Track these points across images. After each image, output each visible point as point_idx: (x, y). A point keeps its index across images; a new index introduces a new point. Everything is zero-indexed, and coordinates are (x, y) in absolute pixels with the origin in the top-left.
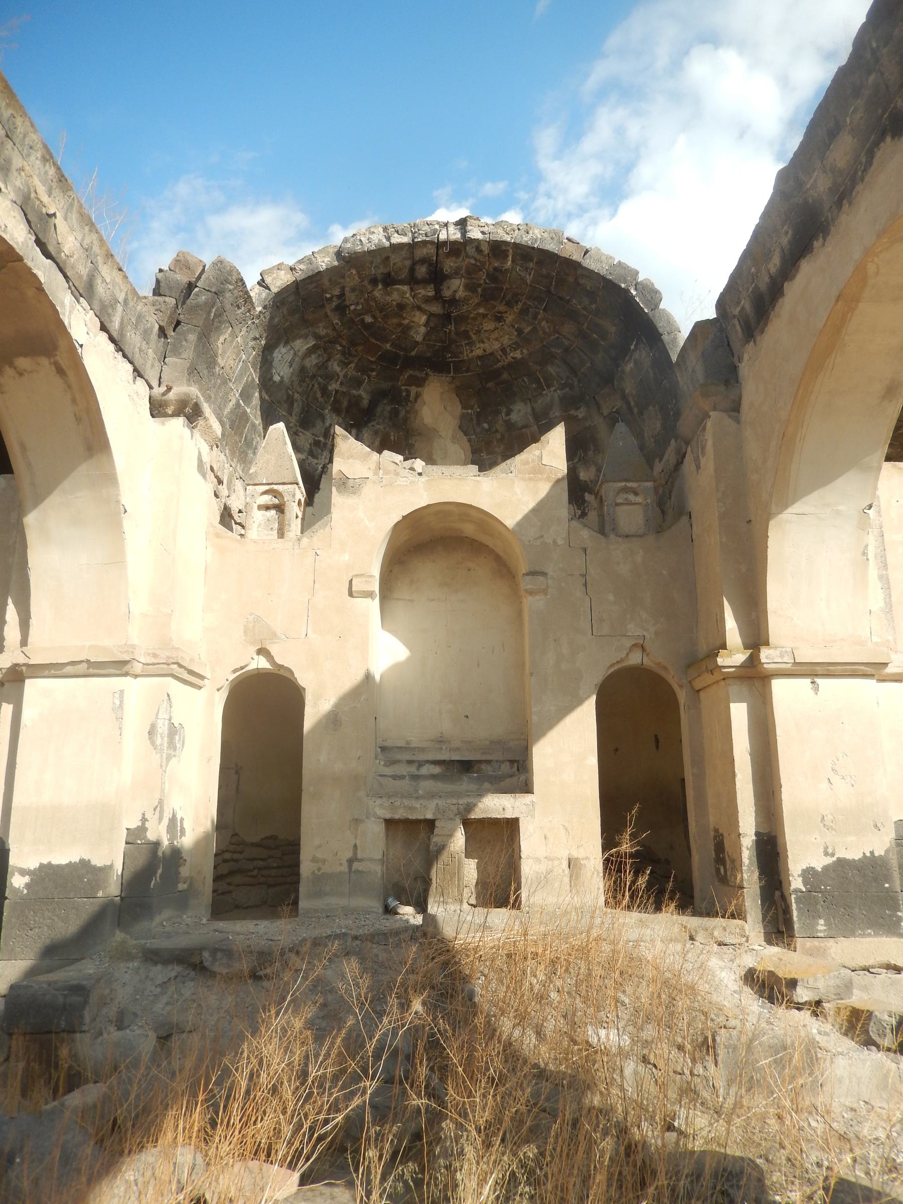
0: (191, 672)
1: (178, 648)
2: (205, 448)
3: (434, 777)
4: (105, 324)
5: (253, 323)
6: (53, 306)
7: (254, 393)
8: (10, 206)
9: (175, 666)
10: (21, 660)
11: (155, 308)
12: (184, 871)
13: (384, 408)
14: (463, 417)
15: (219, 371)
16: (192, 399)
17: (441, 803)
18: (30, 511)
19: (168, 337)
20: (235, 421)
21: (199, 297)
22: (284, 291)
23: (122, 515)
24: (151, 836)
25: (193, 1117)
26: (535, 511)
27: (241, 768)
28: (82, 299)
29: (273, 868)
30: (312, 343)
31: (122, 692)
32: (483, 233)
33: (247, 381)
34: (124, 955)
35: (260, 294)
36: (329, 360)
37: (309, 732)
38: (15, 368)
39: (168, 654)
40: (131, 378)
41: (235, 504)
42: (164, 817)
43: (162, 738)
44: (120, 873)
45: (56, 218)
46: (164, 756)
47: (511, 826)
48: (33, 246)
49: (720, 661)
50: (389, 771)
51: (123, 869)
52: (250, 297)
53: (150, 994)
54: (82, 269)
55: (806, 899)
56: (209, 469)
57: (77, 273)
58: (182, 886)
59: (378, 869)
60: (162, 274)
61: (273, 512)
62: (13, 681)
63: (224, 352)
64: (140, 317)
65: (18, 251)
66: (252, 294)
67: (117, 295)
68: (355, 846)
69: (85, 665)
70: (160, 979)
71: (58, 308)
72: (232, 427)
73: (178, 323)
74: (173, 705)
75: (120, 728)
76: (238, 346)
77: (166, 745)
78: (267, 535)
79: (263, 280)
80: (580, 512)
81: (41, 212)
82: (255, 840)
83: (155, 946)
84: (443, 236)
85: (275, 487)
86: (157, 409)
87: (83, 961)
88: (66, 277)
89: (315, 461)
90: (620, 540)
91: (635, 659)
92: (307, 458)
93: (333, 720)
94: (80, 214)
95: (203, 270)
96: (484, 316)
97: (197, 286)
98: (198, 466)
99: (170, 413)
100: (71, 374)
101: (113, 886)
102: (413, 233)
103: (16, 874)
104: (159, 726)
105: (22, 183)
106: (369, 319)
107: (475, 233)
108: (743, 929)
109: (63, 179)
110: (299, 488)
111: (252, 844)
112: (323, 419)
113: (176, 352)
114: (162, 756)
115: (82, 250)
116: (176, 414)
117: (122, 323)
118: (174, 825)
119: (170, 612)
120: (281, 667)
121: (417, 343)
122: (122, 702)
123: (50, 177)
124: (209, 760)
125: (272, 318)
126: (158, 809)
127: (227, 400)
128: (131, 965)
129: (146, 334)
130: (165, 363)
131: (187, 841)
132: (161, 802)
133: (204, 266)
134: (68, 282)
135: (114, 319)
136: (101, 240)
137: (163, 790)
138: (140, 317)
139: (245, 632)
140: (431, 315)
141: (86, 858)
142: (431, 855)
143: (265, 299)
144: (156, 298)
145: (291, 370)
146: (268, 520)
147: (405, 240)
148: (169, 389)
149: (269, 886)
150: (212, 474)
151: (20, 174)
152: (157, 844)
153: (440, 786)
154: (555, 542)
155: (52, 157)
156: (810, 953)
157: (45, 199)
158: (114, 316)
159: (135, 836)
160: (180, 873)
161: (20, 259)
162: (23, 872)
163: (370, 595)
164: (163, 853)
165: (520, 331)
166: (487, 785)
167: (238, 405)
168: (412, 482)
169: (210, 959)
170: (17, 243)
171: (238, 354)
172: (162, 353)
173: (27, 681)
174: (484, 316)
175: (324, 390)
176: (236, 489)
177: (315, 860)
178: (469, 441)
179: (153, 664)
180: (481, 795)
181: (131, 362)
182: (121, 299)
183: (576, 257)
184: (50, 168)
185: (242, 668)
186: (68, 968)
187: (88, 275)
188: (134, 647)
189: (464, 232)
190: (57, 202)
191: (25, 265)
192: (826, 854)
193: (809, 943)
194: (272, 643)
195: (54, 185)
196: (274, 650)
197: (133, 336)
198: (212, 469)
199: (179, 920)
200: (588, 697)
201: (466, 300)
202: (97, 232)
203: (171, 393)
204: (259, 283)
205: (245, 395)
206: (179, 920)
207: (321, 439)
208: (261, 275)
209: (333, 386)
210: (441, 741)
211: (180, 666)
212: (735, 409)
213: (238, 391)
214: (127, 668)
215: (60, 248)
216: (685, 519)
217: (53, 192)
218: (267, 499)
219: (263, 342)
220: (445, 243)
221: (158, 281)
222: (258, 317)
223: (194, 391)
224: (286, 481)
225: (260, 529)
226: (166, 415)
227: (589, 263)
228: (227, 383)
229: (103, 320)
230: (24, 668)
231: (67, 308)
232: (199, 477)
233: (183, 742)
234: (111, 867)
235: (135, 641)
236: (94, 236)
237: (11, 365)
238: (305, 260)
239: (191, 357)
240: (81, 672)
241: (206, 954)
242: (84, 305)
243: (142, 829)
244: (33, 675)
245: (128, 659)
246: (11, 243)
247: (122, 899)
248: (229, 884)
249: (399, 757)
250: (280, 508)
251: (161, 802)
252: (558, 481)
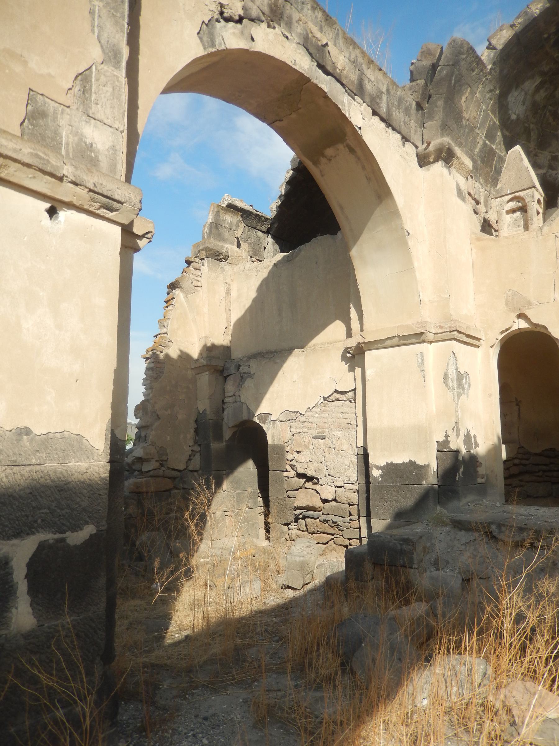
0: (468, 336)
1: (456, 320)
2: (461, 180)
4: (376, 110)
5: (487, 79)
6: (336, 106)
7: (496, 133)
8: (296, 47)
9: (455, 332)
10: (361, 340)
11: (411, 91)
12: (481, 470)
15: (466, 123)
16: (445, 146)
18: (352, 248)
19: (425, 109)
20: (485, 157)
21: (442, 72)
22: (509, 45)
23: (407, 237)
24: (453, 446)
25: (471, 642)
27: (520, 402)
28: (356, 97)
29: (554, 471)
30: (538, 80)
31: (422, 353)
33: (489, 125)
34: (440, 522)
35: (489, 56)
38: (326, 158)
39: (449, 325)
40: (401, 143)
41: (492, 217)
42: (461, 434)
43: (452, 382)
44: (435, 470)
45: (328, 46)
46: (456, 393)
48: (316, 70)
51: (437, 468)
52: (480, 59)
53: (458, 549)
54: (353, 77)
56: (467, 194)
57: (350, 80)
58: (480, 480)
60: (413, 66)
61: (518, 213)
62: (359, 354)
63: (467, 108)
64: (400, 100)
65: (306, 75)
66: (483, 58)
67: (381, 89)
69: (397, 339)
70: (464, 541)
71: (340, 107)
72: (482, 162)
73: (430, 97)
74: (458, 359)
75: (424, 377)
76: (477, 101)
77: (456, 386)
78: (516, 231)
79: (490, 44)
81: (318, 45)
82: (538, 451)
83: (458, 518)
85: (518, 194)
87: (417, 524)
88: (343, 85)
92: (548, 172)
94: (345, 38)
95: (442, 52)
97: (439, 66)
98: (458, 193)
99: (432, 160)
100: (358, 150)
101: (431, 478)
103: (374, 468)
104: (449, 374)
105: (301, 29)
109: (328, 18)
110: (537, 190)
111: (536, 454)
114: (454, 394)
115: (350, 64)
116: (436, 160)
117: (388, 107)
118: (468, 439)
119: (448, 297)
120: (537, 325)
122: (422, 360)
123: (319, 19)
124: (490, 395)
125: (501, 71)
126: (455, 429)
127: (475, 143)
128: (444, 529)
129: (407, 111)
130: (424, 128)
132: (457, 424)
133: (442, 48)
134: (344, 88)
135: (381, 105)
136: (363, 53)
137: (457, 416)
138: (400, 100)
139: (507, 304)
141: (413, 460)
143: (493, 58)
144: (411, 84)
145: (525, 107)
146: (516, 220)
148: (429, 144)
150: (470, 198)
151: (299, 24)
152: (457, 452)
155: (318, 5)
157: (318, 35)
158: (381, 103)
159: (442, 446)
160: (478, 472)
161: (308, 80)
162: (378, 468)
164: (463, 457)
167: (485, 144)
169: (497, 531)
170: (305, 70)
171: (479, 106)
172: (421, 122)
173: (366, 353)
176: (492, 206)
179: (441, 333)
181: (399, 132)
182: (384, 89)
184: (318, 13)
185: (507, 330)
186: (406, 527)
187: (358, 79)
188: (426, 323)
190: (327, 35)
191: (313, 83)
194: (528, 309)
195: (323, 24)
196: (530, 313)
197: (398, 114)
198: (469, 194)
199: (481, 502)
202: (359, 48)
203: (430, 147)
204: (488, 48)
205: (490, 136)
206: (481, 502)
208: (488, 40)
211: (459, 332)
213: (483, 134)
214: (423, 337)
215: (335, 67)
217: (323, 29)
219: (497, 92)
221: (411, 72)
222: (490, 73)
223: (446, 140)
224: (525, 187)
225: (510, 228)
226: (430, 163)
228: (473, 130)
229: (373, 108)
230: (363, 345)
231: (347, 105)
232: (460, 202)
233: (469, 384)
234: (428, 466)
235: (428, 320)
236: (357, 51)
237: (323, 156)
238: (521, 14)
239: (441, 117)
240: (396, 344)
242: (358, 101)
243: (446, 442)
244: (369, 349)
245: (422, 331)
246: (300, 71)
247: (439, 486)
248: (521, 481)
250: (523, 209)
251: (457, 424)
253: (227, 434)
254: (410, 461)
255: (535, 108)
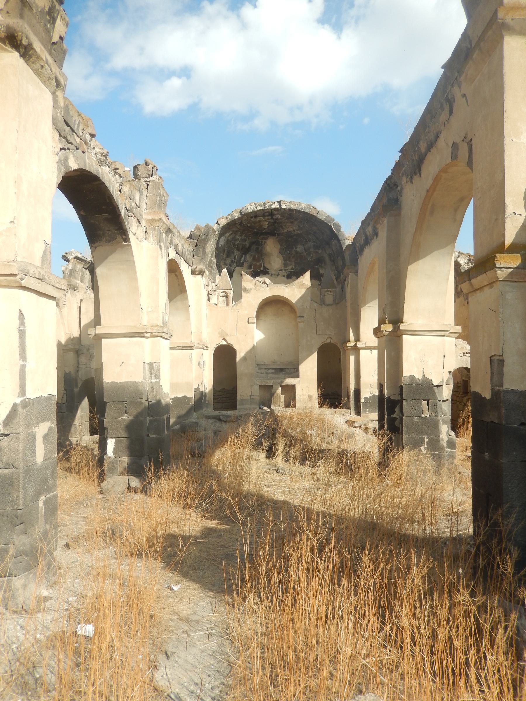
3: (272, 373)
12: (207, 399)
13: (254, 247)
14: (281, 249)
17: (274, 381)
24: (201, 390)
26: (301, 298)
30: (231, 232)
31: (191, 354)
32: (286, 206)
35: (217, 227)
36: (236, 235)
37: (238, 362)
47: (293, 387)
49: (347, 345)
50: (260, 371)
55: (365, 404)
58: (207, 402)
59: (258, 398)
61: (225, 298)
68: (252, 392)
79: (218, 222)
80: (319, 283)
84: (273, 207)
86: (193, 273)
89: (231, 267)
90: (325, 306)
91: (329, 341)
93: (244, 358)
96: (287, 222)
102: (264, 206)
106: (249, 225)
107: (283, 206)
108: (348, 411)
112: (234, 253)
113: (197, 255)
116: (198, 274)
121: (265, 229)
131: (207, 391)
132: (203, 381)
139: (219, 334)
140: (269, 222)
142: (272, 394)
147: (261, 208)
149: (223, 403)
152: (203, 392)
153: (274, 375)
154: (307, 307)
156: (363, 417)
159: (197, 390)
163: (253, 323)
165: (299, 227)
166: (287, 375)
168: (265, 289)
174: (287, 222)
175: (234, 244)
177: (241, 396)
178: (283, 257)
180: (285, 379)
183: (315, 214)
189: (280, 206)
192: (370, 394)
193: (364, 415)
196: (227, 339)
200: (315, 352)
201: (281, 219)
207: (233, 260)
209: (237, 243)
210: (274, 362)
212: (357, 272)
216: (344, 300)
218: (223, 294)
220: (274, 209)
226: (196, 274)
227: (320, 217)
241: (221, 417)
243: (198, 388)
249: (262, 367)
250: (227, 297)
252: (308, 288)
253: (80, 384)
254: (185, 396)
255: (228, 241)
